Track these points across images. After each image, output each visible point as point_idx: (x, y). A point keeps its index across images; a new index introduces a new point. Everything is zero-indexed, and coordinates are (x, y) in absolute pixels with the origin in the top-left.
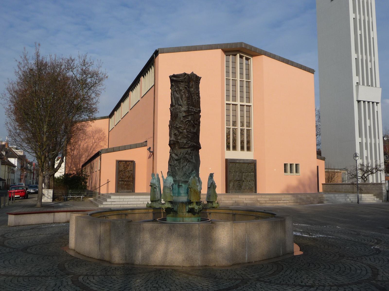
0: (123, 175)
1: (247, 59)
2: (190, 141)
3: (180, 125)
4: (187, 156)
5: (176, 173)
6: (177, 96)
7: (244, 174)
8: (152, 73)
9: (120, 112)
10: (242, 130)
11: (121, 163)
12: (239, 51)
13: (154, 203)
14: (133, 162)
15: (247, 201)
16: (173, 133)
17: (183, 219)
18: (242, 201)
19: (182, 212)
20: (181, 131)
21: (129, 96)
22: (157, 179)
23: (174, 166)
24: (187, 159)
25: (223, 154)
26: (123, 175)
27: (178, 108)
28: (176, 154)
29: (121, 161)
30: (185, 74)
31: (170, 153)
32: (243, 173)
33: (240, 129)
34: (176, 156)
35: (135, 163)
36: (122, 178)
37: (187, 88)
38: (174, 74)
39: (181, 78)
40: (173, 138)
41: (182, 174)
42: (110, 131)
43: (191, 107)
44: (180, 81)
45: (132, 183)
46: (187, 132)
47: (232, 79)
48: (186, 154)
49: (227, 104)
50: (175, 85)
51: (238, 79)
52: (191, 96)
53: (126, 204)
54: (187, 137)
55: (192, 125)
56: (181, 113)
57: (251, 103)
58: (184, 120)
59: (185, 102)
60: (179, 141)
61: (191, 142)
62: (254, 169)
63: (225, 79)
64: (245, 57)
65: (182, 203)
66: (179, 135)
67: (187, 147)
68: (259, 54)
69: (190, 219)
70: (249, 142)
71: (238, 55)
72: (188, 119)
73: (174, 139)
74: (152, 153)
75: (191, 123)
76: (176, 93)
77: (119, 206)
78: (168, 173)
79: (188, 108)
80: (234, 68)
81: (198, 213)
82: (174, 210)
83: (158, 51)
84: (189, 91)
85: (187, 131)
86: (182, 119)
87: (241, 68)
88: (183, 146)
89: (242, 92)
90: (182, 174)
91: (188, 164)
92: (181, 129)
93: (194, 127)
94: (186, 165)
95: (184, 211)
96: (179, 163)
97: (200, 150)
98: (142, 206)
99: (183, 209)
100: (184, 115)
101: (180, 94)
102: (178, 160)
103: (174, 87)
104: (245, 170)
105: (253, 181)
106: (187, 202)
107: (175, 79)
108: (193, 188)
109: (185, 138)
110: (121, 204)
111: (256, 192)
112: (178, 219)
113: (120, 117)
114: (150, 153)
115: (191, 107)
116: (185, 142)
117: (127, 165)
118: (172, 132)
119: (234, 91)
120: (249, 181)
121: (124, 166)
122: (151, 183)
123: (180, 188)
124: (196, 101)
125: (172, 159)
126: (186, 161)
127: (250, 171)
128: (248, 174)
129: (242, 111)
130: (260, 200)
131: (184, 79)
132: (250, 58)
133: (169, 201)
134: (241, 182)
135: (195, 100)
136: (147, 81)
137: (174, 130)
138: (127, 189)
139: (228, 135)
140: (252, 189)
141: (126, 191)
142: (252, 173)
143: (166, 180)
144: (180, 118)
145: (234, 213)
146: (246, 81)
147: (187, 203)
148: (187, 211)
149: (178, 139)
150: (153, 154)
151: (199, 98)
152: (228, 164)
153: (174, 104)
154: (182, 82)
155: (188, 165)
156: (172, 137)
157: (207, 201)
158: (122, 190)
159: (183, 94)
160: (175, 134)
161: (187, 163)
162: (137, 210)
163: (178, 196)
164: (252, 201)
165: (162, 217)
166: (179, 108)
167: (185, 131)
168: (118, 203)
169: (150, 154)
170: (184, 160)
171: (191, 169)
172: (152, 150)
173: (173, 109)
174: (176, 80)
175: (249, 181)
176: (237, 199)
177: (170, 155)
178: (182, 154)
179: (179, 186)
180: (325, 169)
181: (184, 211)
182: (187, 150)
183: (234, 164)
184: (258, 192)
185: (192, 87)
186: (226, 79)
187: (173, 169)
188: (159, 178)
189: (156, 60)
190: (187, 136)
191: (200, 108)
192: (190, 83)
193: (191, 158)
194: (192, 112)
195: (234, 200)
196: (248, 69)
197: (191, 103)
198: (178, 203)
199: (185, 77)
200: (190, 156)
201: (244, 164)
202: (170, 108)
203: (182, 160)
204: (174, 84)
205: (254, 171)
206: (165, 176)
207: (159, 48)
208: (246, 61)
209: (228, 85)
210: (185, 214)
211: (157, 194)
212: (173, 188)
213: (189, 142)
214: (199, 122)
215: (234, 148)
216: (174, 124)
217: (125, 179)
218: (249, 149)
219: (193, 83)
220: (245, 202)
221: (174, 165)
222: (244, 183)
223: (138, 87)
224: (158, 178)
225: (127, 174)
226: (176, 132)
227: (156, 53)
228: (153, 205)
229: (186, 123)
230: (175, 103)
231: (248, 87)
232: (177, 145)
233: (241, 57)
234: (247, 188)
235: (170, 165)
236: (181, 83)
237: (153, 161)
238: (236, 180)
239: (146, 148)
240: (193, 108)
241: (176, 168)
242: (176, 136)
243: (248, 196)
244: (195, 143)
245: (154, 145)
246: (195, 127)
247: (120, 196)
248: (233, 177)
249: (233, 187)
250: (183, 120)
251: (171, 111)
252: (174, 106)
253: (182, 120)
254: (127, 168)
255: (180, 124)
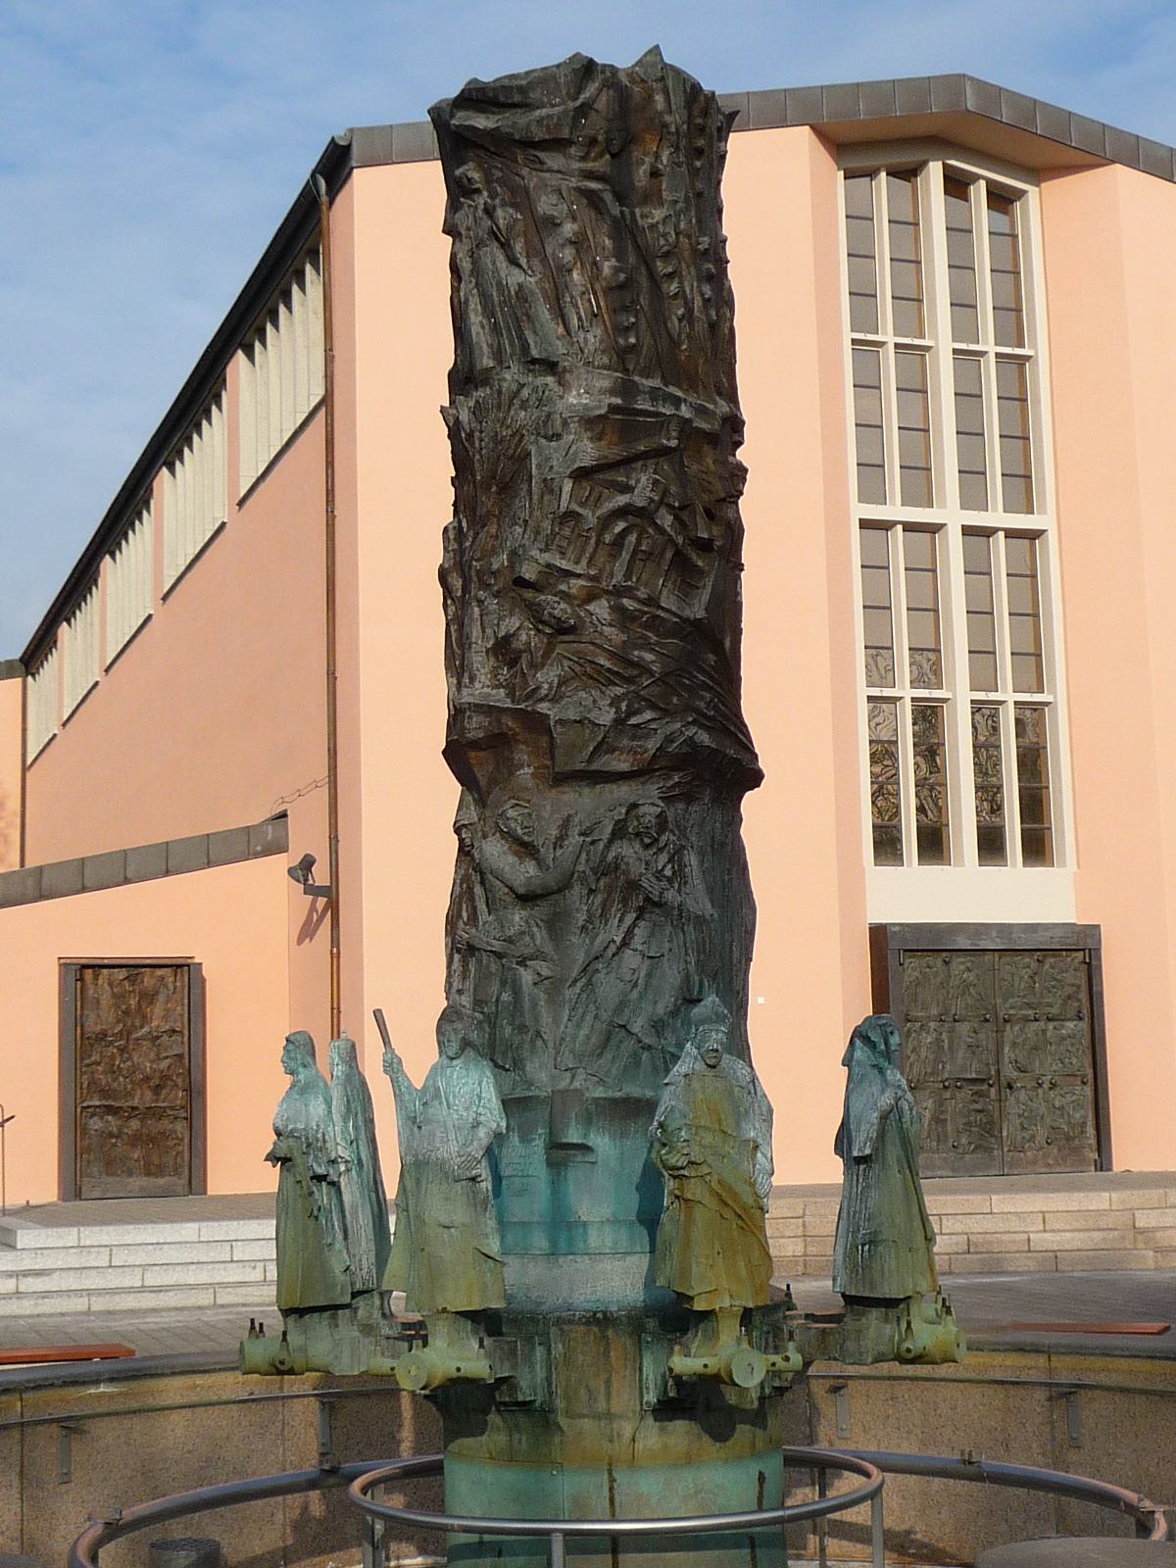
0: (113, 1071)
1: (1001, 200)
2: (653, 707)
3: (546, 557)
4: (628, 851)
5: (522, 1029)
6: (514, 278)
7: (1010, 1033)
8: (311, 316)
9: (97, 628)
10: (985, 714)
11: (96, 977)
12: (938, 142)
13: (319, 1324)
14: (184, 970)
15: (1057, 1237)
16: (480, 642)
17: (612, 1480)
18: (1017, 1237)
19: (597, 1417)
20: (561, 609)
21: (152, 502)
22: (336, 1094)
23: (499, 955)
24: (633, 886)
25: (851, 891)
26: (113, 1071)
27: (525, 393)
28: (523, 844)
29: (96, 967)
30: (586, 69)
31: (457, 831)
32: (1008, 1026)
33: (972, 702)
34: (516, 854)
35: (203, 981)
36: (104, 1093)
37: (608, 197)
38: (475, 81)
39: (542, 106)
40: (483, 688)
41: (584, 1032)
42: (29, 762)
43: (656, 383)
44: (539, 134)
45: (180, 1127)
46: (623, 618)
47: (897, 346)
48: (619, 832)
49: (865, 524)
50: (488, 180)
51: (942, 339)
52: (652, 275)
53: (130, 1290)
54: (627, 669)
55: (669, 555)
56: (557, 436)
57: (1043, 512)
58: (582, 505)
59: (593, 338)
60: (543, 707)
61: (666, 713)
62: (1084, 996)
63: (848, 346)
64: (983, 184)
65: (601, 1320)
66: (546, 655)
67: (625, 767)
68: (1090, 159)
69: (688, 1479)
70: (1034, 805)
71: (935, 171)
72: (622, 500)
73: (500, 698)
74: (322, 901)
75: (660, 530)
76: (500, 256)
77: (79, 1304)
78: (448, 1027)
79: (627, 389)
80: (909, 262)
81: (758, 1418)
82: (521, 1398)
83: (348, 147)
84: (625, 232)
85: (618, 610)
86: (565, 496)
87: (961, 266)
88: (590, 761)
89: (970, 433)
90: (584, 1032)
91: (640, 933)
92: (565, 596)
93: (684, 572)
94: (625, 943)
95: (624, 1400)
96: (556, 925)
97: (750, 801)
98: (257, 1300)
99: (608, 1382)
100: (587, 462)
101: (544, 260)
102: (542, 896)
103: (483, 199)
104: (1019, 1001)
105: (1084, 1083)
106: (649, 1310)
107: (482, 122)
108: (705, 1170)
109: (601, 678)
110: (89, 1292)
111: (1103, 1163)
112: (567, 1485)
113: (96, 654)
114: (314, 902)
115: (656, 383)
116: (606, 717)
117: (143, 995)
118: (476, 633)
119: (918, 431)
120: (1053, 1086)
121: (119, 998)
122: (279, 1134)
123: (574, 1175)
124: (701, 327)
125: (478, 890)
126: (625, 901)
127: (1054, 1011)
128: (1044, 1032)
129: (978, 569)
130: (1153, 1224)
131: (575, 120)
132: (1023, 193)
133: (457, 1313)
134: (993, 1090)
135: (689, 316)
136: (274, 380)
137: (492, 604)
138: (148, 1174)
139: (883, 754)
140: (1076, 1142)
141: (138, 1182)
142: (1071, 1025)
143: (431, 1094)
144: (550, 488)
145: (1065, 1378)
146: (998, 355)
147: (651, 1324)
148: (651, 1397)
149: (538, 688)
150: (333, 906)
151: (722, 300)
152: (892, 962)
153: (487, 362)
154: (557, 144)
155: (637, 941)
156: (472, 679)
157: (844, 1295)
158: (111, 1179)
159: (567, 255)
160: (504, 650)
161: (634, 925)
162: (174, 1374)
163: (553, 1253)
164: (1097, 1235)
165: (407, 1454)
166: (535, 389)
167: (601, 609)
168: (71, 1282)
169: (313, 908)
170: (599, 899)
171: (671, 977)
172: (320, 876)
173: (477, 411)
174: (492, 134)
175: (1053, 1086)
176: (975, 1225)
177: (464, 851)
178: (574, 839)
179: (560, 1154)
180: (866, 647)
181: (624, 1400)
182: (624, 792)
183: (939, 962)
184: (1118, 1166)
185: (651, 197)
186: (854, 342)
187: (495, 987)
188: (364, 1084)
189: (336, 217)
190: (631, 664)
191: (732, 396)
192: (636, 154)
193: (668, 872)
194: (661, 423)
195: (959, 1228)
196: (1010, 271)
197: (648, 340)
198: (559, 1321)
199: (582, 98)
200: (663, 858)
201: (1008, 959)
202: (443, 410)
203: (577, 891)
204: (476, 176)
205: (1085, 1012)
206: (420, 1053)
207: (351, 130)
208: (995, 214)
209: (867, 385)
210: (627, 1430)
211: (339, 1245)
212: (497, 1179)
213: (648, 715)
214: (734, 532)
215: (934, 844)
216: (494, 552)
217: (129, 1094)
218: (1037, 848)
219: (657, 156)
220: (1044, 1240)
221: (497, 946)
222: (1018, 1100)
223: (212, 437)
224: (348, 1078)
225: (145, 1061)
226: (512, 623)
227: (336, 165)
228: (303, 1349)
229: (608, 538)
230: (498, 355)
231: (1017, 399)
232: (522, 754)
233: (956, 186)
234: (1041, 1138)
235: (462, 949)
236: (542, 155)
237: (335, 957)
238: (958, 1080)
239: (280, 863)
240: (672, 389)
241: (526, 977)
242: (513, 663)
243: (1061, 1195)
244: (702, 721)
245: (334, 839)
246: (701, 573)
247: (88, 1225)
248: (931, 1057)
249: (934, 1136)
250: (575, 507)
251: (454, 434)
252: (483, 379)
253: (564, 504)
254: (144, 1017)
255: (546, 549)
